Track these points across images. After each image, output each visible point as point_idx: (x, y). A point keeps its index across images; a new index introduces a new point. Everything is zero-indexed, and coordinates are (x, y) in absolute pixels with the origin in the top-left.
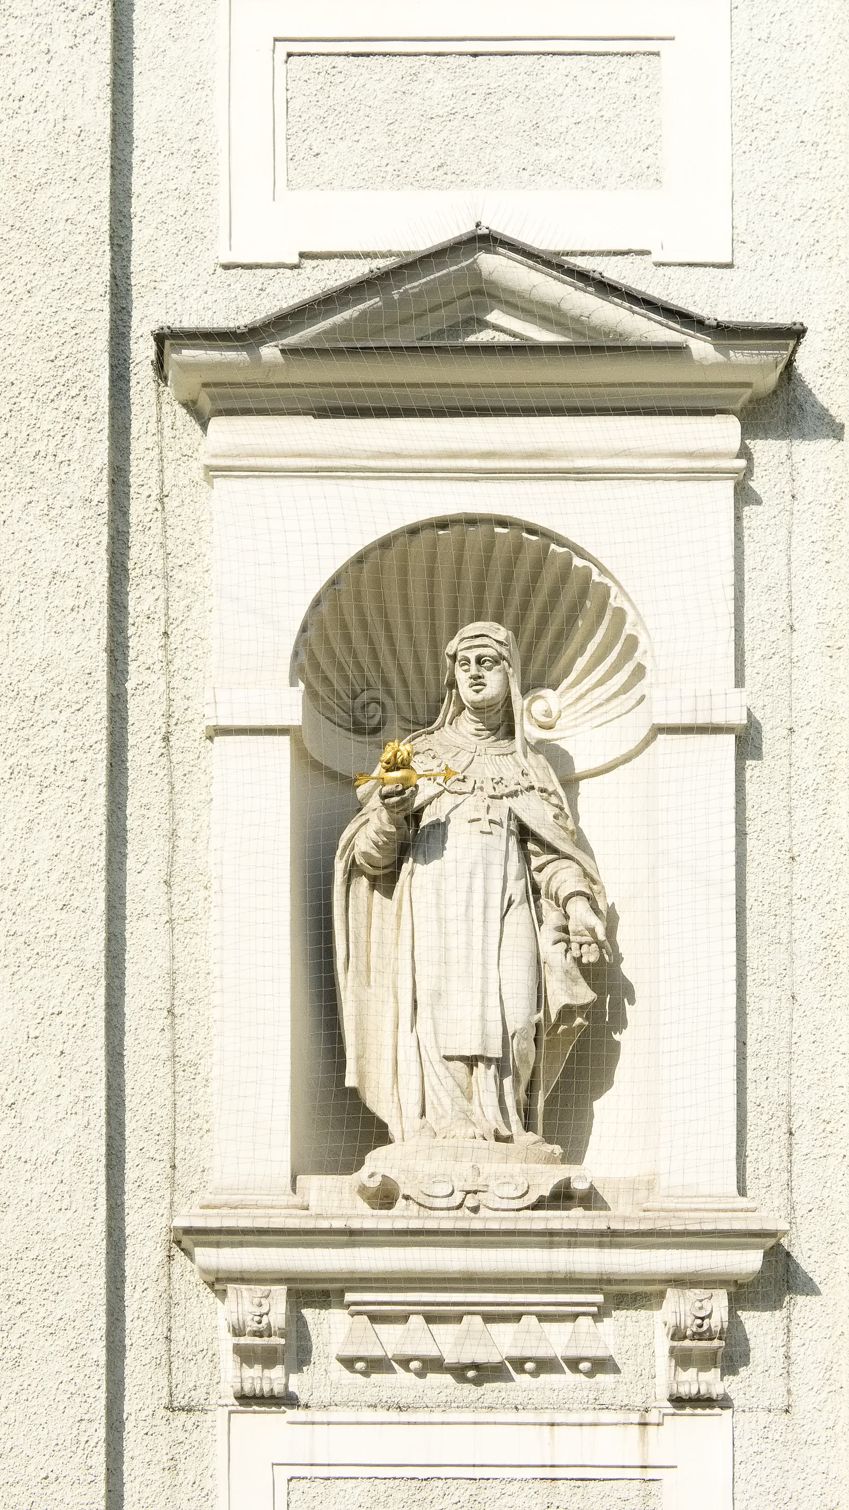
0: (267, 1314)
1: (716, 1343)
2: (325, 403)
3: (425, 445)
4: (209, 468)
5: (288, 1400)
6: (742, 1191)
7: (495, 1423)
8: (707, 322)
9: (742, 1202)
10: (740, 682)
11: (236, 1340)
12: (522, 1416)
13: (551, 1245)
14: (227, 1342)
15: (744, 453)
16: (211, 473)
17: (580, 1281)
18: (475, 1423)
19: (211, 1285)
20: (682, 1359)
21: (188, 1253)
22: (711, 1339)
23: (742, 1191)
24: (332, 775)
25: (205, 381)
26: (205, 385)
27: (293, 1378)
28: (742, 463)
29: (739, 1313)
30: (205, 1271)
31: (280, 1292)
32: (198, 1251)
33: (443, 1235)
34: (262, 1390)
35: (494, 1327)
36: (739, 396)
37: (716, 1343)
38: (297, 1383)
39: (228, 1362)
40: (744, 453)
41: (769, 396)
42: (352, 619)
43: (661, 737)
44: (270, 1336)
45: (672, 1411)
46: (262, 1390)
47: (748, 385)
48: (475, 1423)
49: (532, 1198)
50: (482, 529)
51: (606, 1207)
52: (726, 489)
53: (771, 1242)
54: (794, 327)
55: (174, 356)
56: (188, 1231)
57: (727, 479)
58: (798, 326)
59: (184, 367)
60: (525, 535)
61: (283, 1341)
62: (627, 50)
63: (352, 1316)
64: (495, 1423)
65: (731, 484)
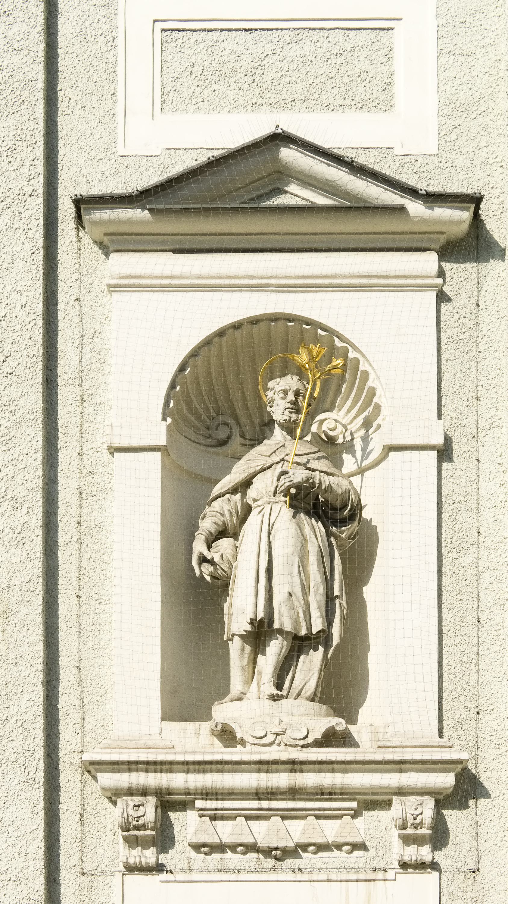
0: (421, 814)
1: (149, 832)
2: (178, 247)
3: (347, 270)
4: (110, 286)
5: (159, 868)
6: (441, 736)
7: (268, 881)
8: (420, 192)
9: (441, 741)
10: (440, 416)
11: (125, 833)
12: (242, 877)
13: (119, 771)
14: (396, 833)
15: (441, 274)
16: (111, 289)
17: (237, 794)
18: (167, 882)
19: (110, 798)
20: (407, 840)
21: (95, 778)
22: (146, 829)
23: (441, 736)
24: (198, 477)
25: (106, 232)
26: (105, 234)
27: (162, 856)
28: (440, 281)
29: (170, 814)
30: (104, 789)
31: (152, 801)
32: (99, 775)
33: (450, 764)
34: (140, 862)
35: (321, 822)
36: (439, 239)
37: (149, 832)
38: (164, 859)
39: (396, 844)
40: (441, 274)
41: (465, 237)
42: (202, 381)
43: (391, 454)
44: (421, 828)
45: (401, 871)
46: (140, 862)
47: (443, 233)
48: (167, 882)
49: (310, 740)
50: (281, 323)
51: (356, 745)
52: (432, 296)
53: (459, 767)
54: (475, 196)
55: (88, 217)
56: (92, 763)
57: (432, 290)
58: (478, 195)
59: (93, 223)
60: (304, 326)
61: (154, 833)
62: (280, 27)
63: (201, 817)
64: (268, 881)
65: (434, 294)
